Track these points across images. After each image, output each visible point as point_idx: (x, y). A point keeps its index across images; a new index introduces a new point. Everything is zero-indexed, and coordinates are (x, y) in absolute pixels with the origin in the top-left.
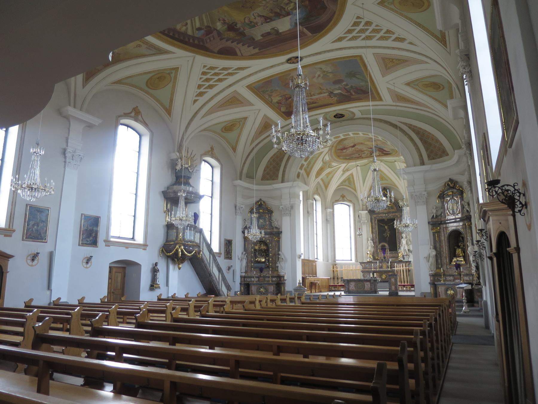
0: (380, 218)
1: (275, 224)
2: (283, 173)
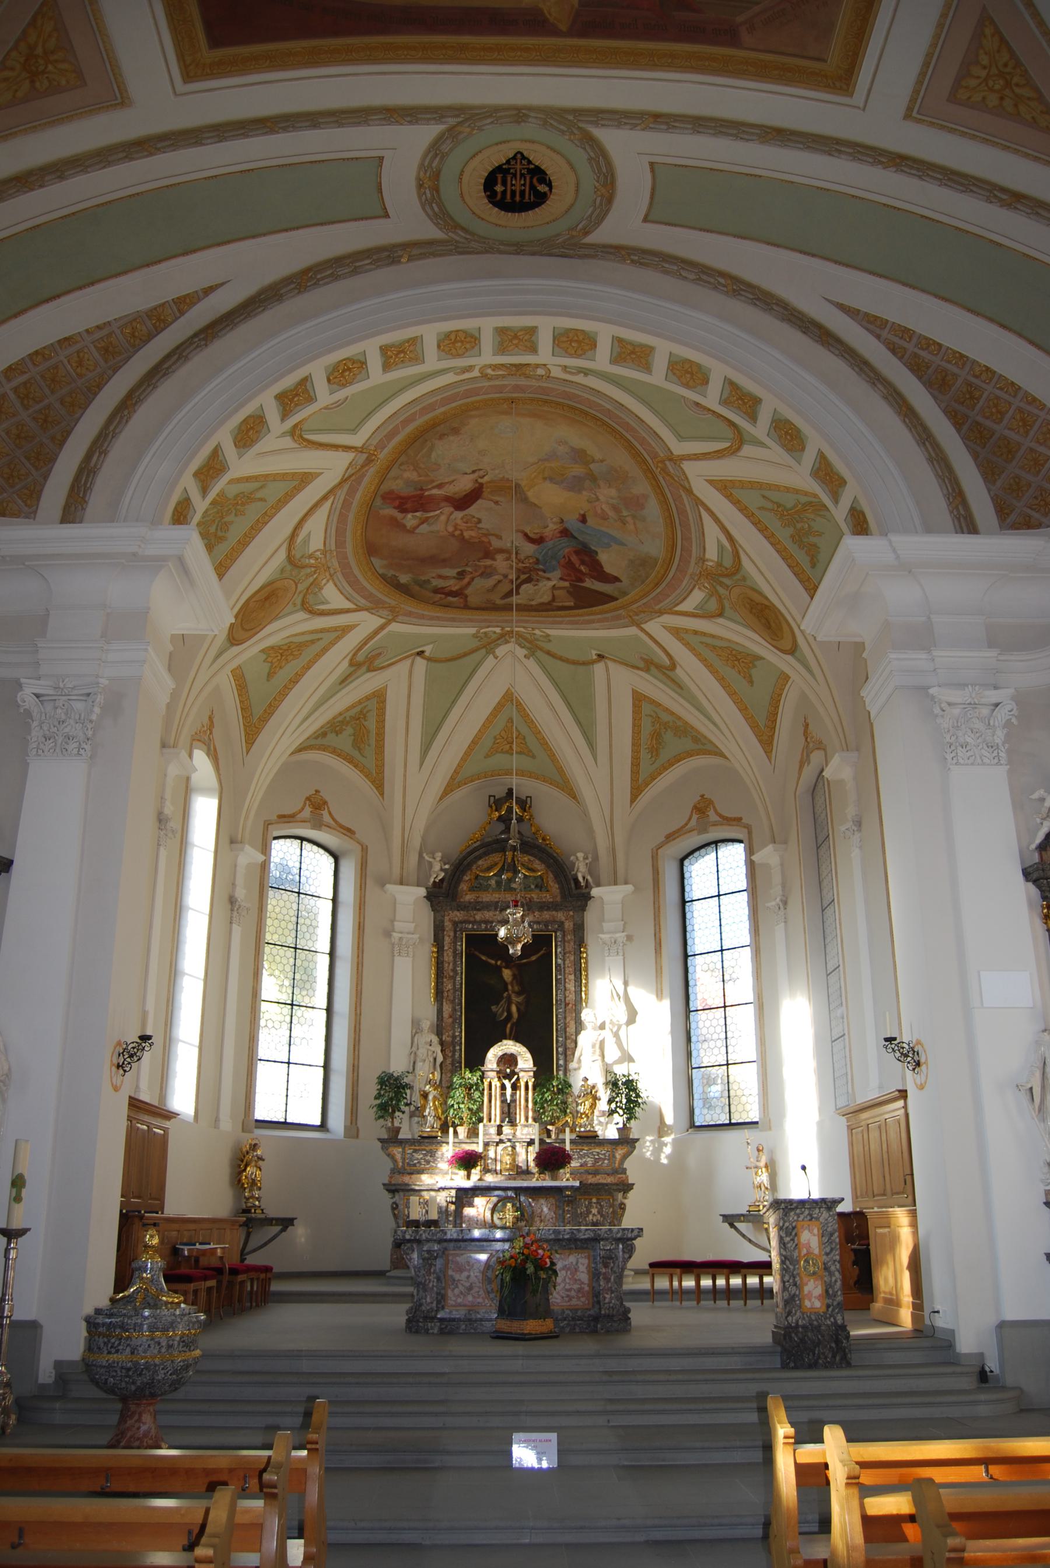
0: (483, 926)
2: (77, 479)
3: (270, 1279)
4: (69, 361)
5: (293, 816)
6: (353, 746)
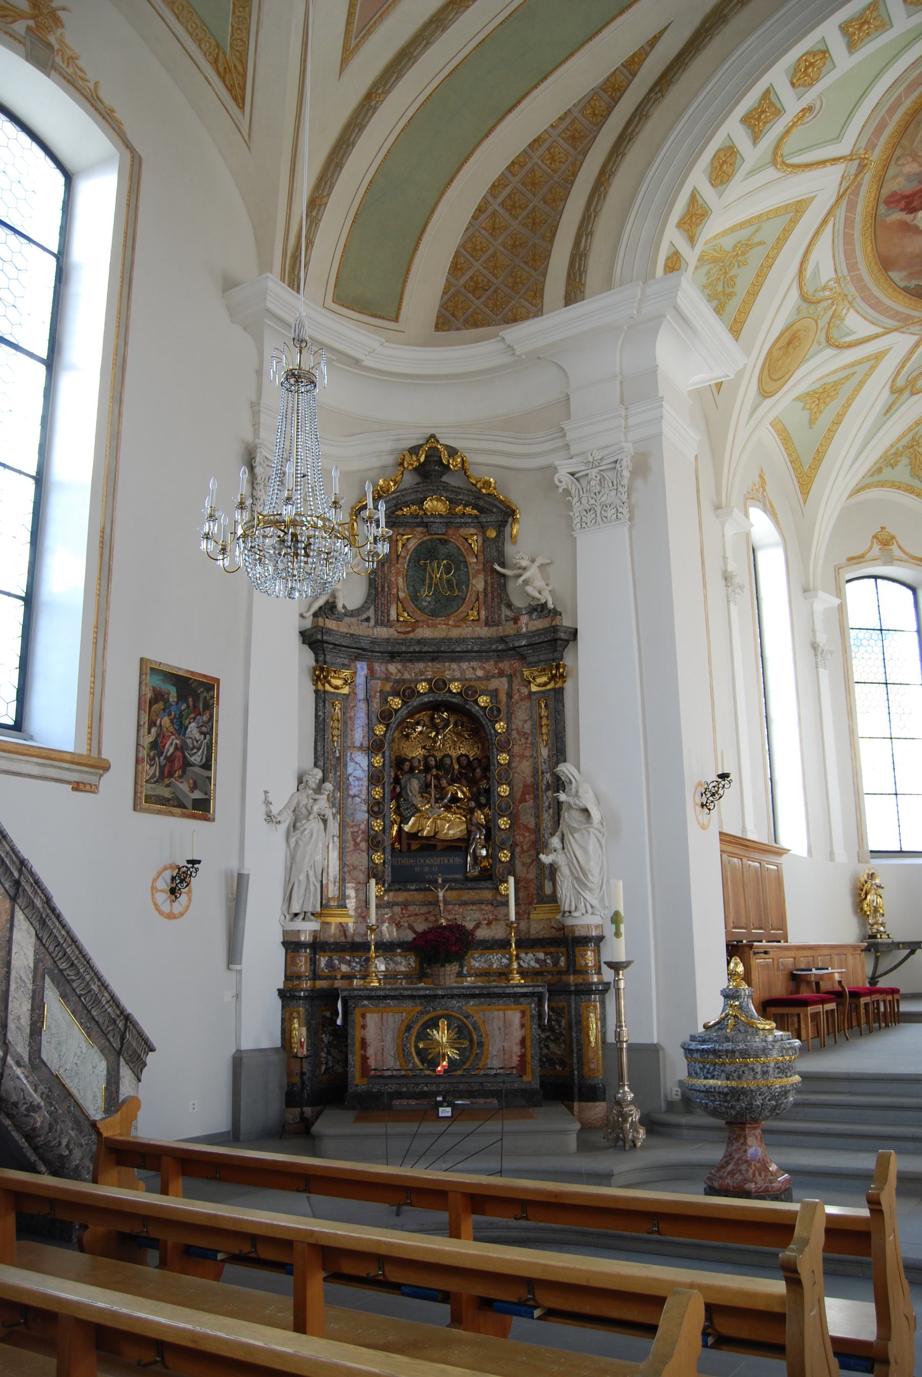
1: (526, 582)
3: (898, 1001)
4: (542, 162)
5: (862, 556)
6: (911, 476)
